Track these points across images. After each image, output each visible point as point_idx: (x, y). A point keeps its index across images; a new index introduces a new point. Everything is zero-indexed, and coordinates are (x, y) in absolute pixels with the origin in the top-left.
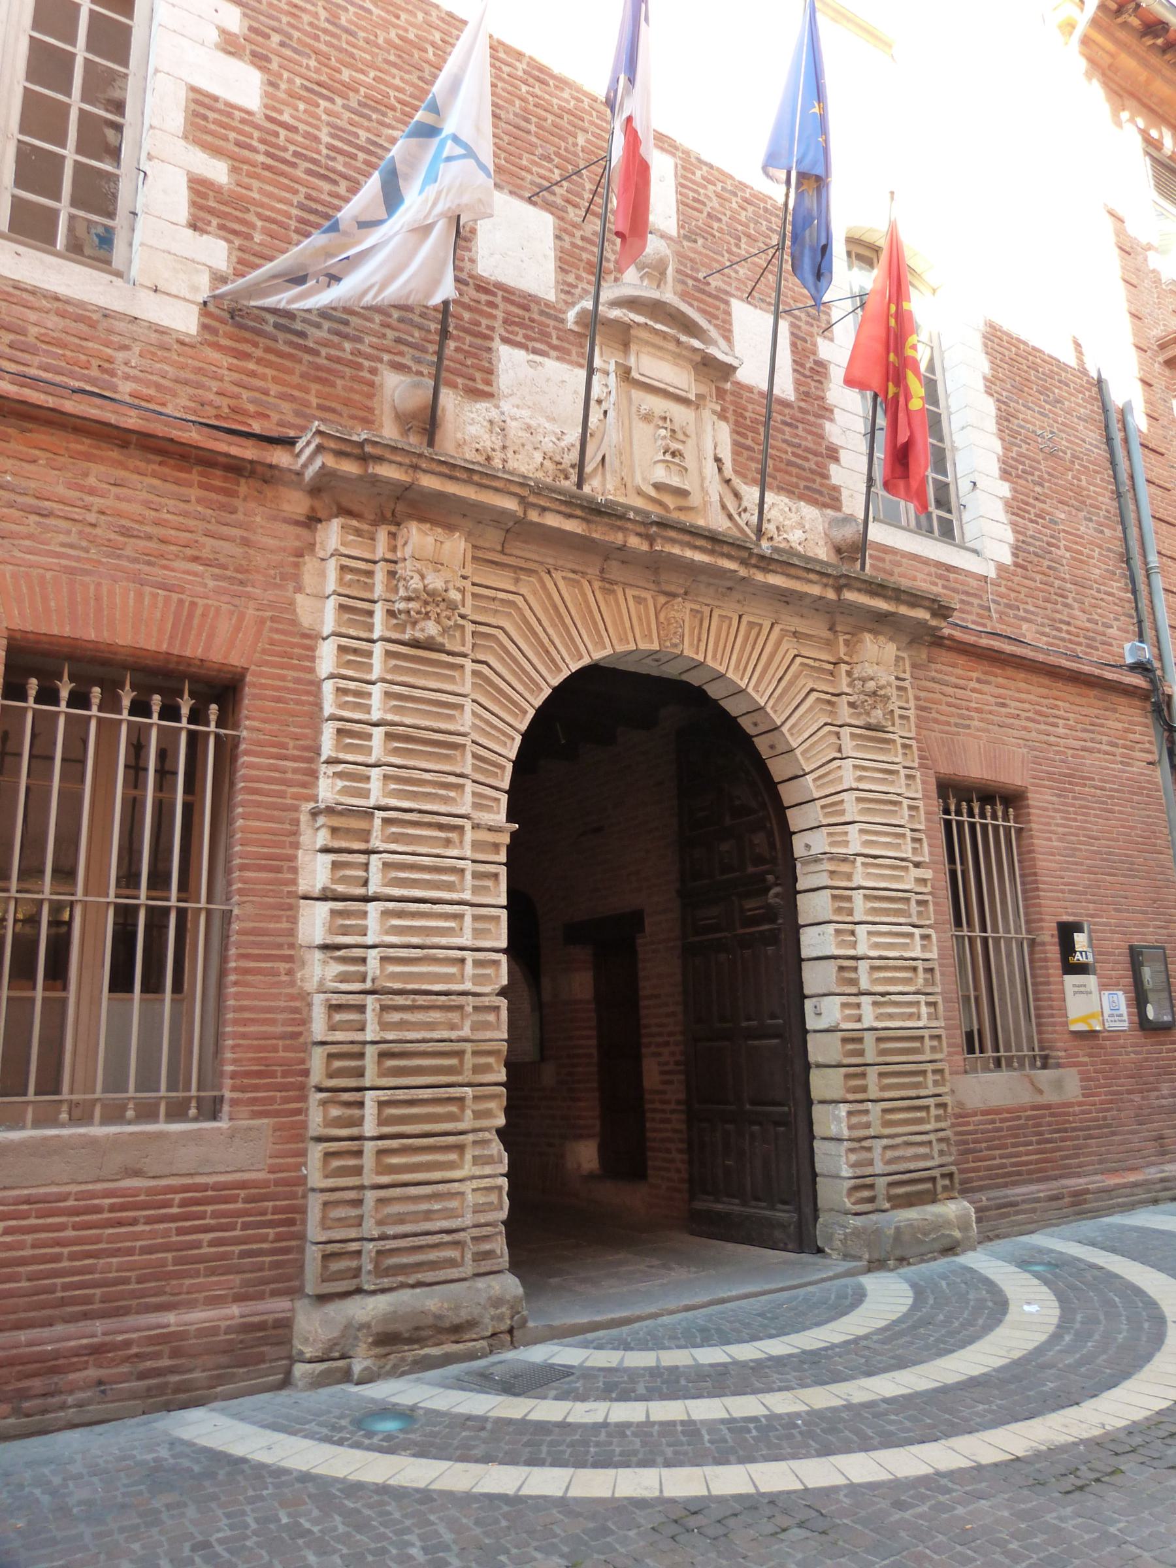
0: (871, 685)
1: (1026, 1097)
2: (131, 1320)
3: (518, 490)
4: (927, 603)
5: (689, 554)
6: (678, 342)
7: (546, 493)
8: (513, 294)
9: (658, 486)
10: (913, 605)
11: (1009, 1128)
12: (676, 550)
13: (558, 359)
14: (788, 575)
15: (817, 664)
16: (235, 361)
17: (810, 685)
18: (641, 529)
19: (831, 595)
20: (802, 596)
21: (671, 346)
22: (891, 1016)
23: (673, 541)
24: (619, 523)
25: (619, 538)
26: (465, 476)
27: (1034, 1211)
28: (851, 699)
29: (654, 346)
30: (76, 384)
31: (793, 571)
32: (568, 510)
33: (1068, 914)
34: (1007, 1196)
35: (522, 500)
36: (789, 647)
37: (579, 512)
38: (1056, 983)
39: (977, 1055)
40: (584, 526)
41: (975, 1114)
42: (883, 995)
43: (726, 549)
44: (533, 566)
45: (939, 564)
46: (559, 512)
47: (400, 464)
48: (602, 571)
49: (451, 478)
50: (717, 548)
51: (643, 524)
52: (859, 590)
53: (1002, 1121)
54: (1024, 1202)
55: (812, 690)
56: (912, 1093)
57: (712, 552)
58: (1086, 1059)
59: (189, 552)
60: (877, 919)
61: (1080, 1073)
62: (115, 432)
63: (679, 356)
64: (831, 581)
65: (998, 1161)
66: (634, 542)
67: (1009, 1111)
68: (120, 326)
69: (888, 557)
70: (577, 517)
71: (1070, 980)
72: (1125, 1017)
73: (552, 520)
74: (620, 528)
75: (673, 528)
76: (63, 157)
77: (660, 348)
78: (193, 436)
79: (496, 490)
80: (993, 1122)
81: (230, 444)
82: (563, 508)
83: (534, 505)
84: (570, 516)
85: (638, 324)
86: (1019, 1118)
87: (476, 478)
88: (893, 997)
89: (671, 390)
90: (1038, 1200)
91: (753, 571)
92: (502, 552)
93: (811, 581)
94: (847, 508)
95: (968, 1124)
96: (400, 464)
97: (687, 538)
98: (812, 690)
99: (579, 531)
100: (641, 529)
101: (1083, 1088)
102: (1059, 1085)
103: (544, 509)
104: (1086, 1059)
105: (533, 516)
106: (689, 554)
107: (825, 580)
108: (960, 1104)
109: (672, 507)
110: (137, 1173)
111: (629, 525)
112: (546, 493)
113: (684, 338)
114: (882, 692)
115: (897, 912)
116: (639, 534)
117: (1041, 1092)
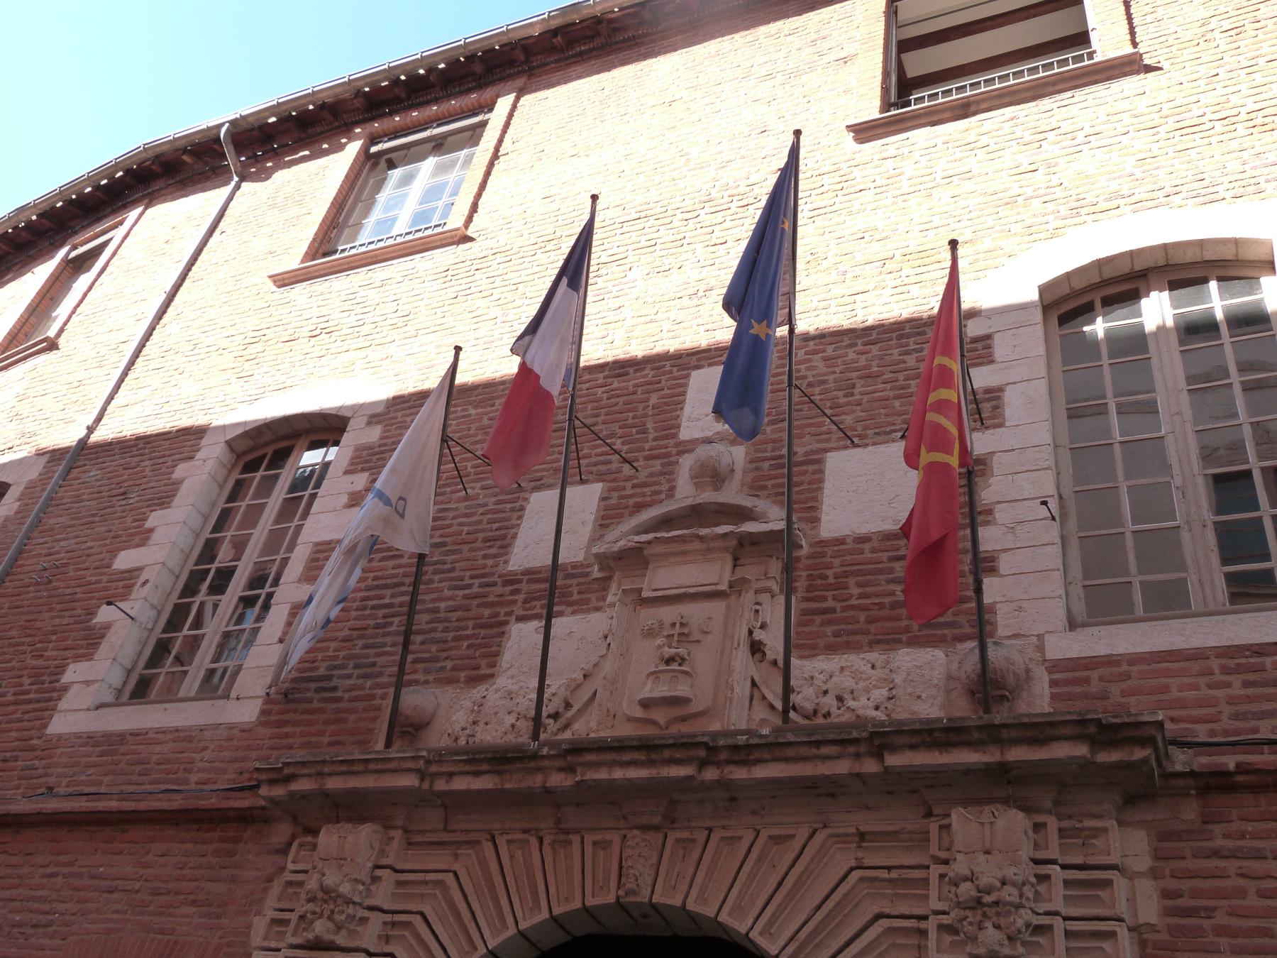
0: (966, 889)
3: (411, 765)
4: (1068, 731)
5: (618, 774)
6: (702, 538)
7: (448, 758)
8: (539, 572)
9: (646, 704)
12: (602, 775)
13: (573, 613)
14: (786, 760)
15: (894, 874)
16: (277, 730)
17: (877, 910)
18: (561, 763)
19: (870, 766)
20: (833, 780)
21: (696, 545)
23: (596, 765)
24: (532, 764)
25: (537, 781)
26: (361, 768)
28: (945, 920)
29: (676, 554)
30: (163, 787)
31: (790, 752)
32: (473, 768)
35: (423, 775)
36: (842, 860)
37: (485, 767)
40: (496, 779)
43: (667, 754)
44: (473, 837)
45: (1226, 652)
46: (467, 773)
47: (309, 775)
48: (558, 821)
49: (352, 773)
50: (654, 756)
51: (559, 756)
52: (913, 747)
55: (879, 916)
57: (651, 763)
59: (192, 897)
63: (709, 550)
64: (863, 748)
66: (557, 780)
68: (207, 734)
69: (1094, 675)
70: (486, 772)
73: (460, 784)
74: (539, 769)
75: (589, 750)
77: (684, 553)
78: (214, 802)
79: (394, 771)
81: (236, 799)
82: (467, 768)
83: (438, 774)
84: (477, 774)
85: (649, 543)
87: (372, 766)
89: (692, 590)
91: (727, 769)
92: (446, 830)
93: (828, 758)
94: (770, 656)
96: (309, 775)
97: (609, 757)
98: (879, 916)
99: (490, 786)
100: (561, 763)
103: (451, 775)
105: (441, 785)
106: (618, 774)
107: (851, 750)
109: (662, 722)
111: (546, 763)
112: (448, 758)
113: (703, 532)
114: (988, 899)
116: (561, 769)
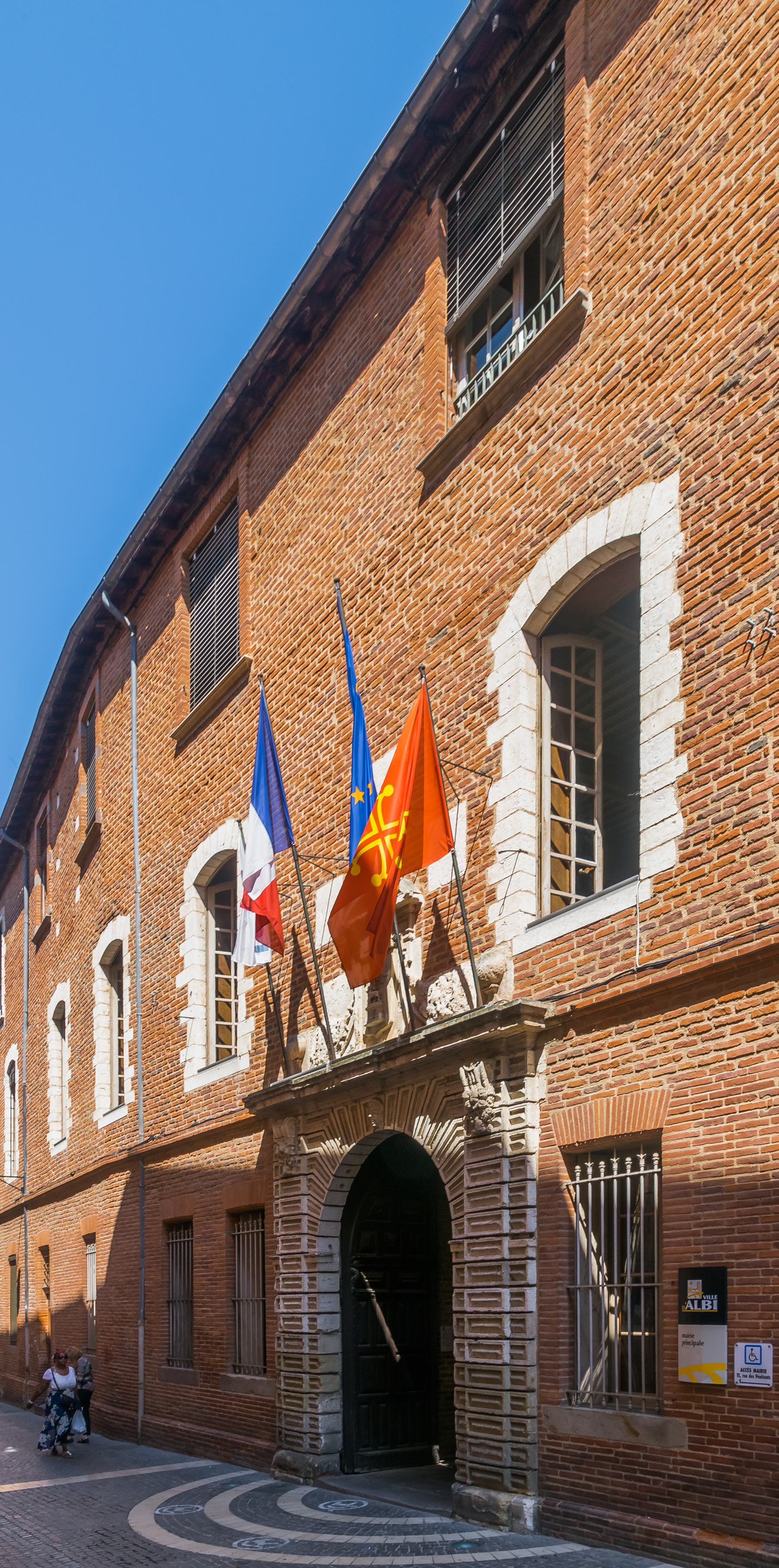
1: (617, 1434)
2: (253, 1440)
10: (393, 1059)
11: (597, 1457)
22: (483, 1355)
27: (600, 1531)
33: (698, 1258)
34: (578, 1510)
38: (669, 1332)
39: (630, 1394)
41: (567, 1439)
42: (476, 1339)
53: (591, 1450)
54: (590, 1519)
56: (490, 1411)
58: (701, 1412)
60: (475, 1285)
61: (689, 1424)
62: (589, 1012)
65: (583, 1482)
67: (598, 1443)
71: (683, 1329)
72: (770, 1373)
76: (578, 856)
80: (582, 1448)
86: (610, 1452)
88: (481, 1341)
90: (606, 1523)
95: (559, 1445)
101: (691, 1440)
102: (660, 1432)
104: (701, 1412)
108: (552, 1428)
110: (252, 1392)
115: (494, 1278)
117: (636, 1434)
